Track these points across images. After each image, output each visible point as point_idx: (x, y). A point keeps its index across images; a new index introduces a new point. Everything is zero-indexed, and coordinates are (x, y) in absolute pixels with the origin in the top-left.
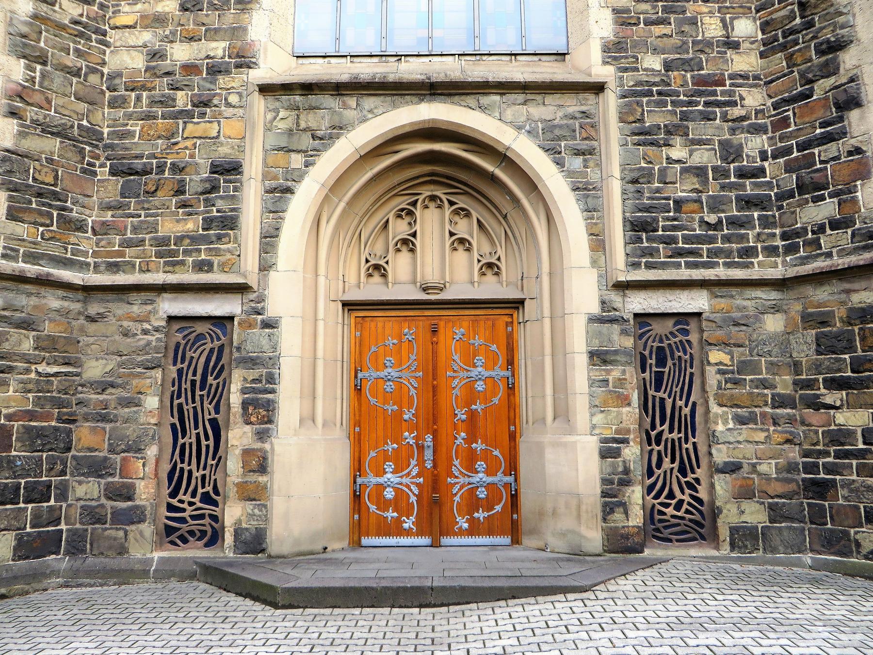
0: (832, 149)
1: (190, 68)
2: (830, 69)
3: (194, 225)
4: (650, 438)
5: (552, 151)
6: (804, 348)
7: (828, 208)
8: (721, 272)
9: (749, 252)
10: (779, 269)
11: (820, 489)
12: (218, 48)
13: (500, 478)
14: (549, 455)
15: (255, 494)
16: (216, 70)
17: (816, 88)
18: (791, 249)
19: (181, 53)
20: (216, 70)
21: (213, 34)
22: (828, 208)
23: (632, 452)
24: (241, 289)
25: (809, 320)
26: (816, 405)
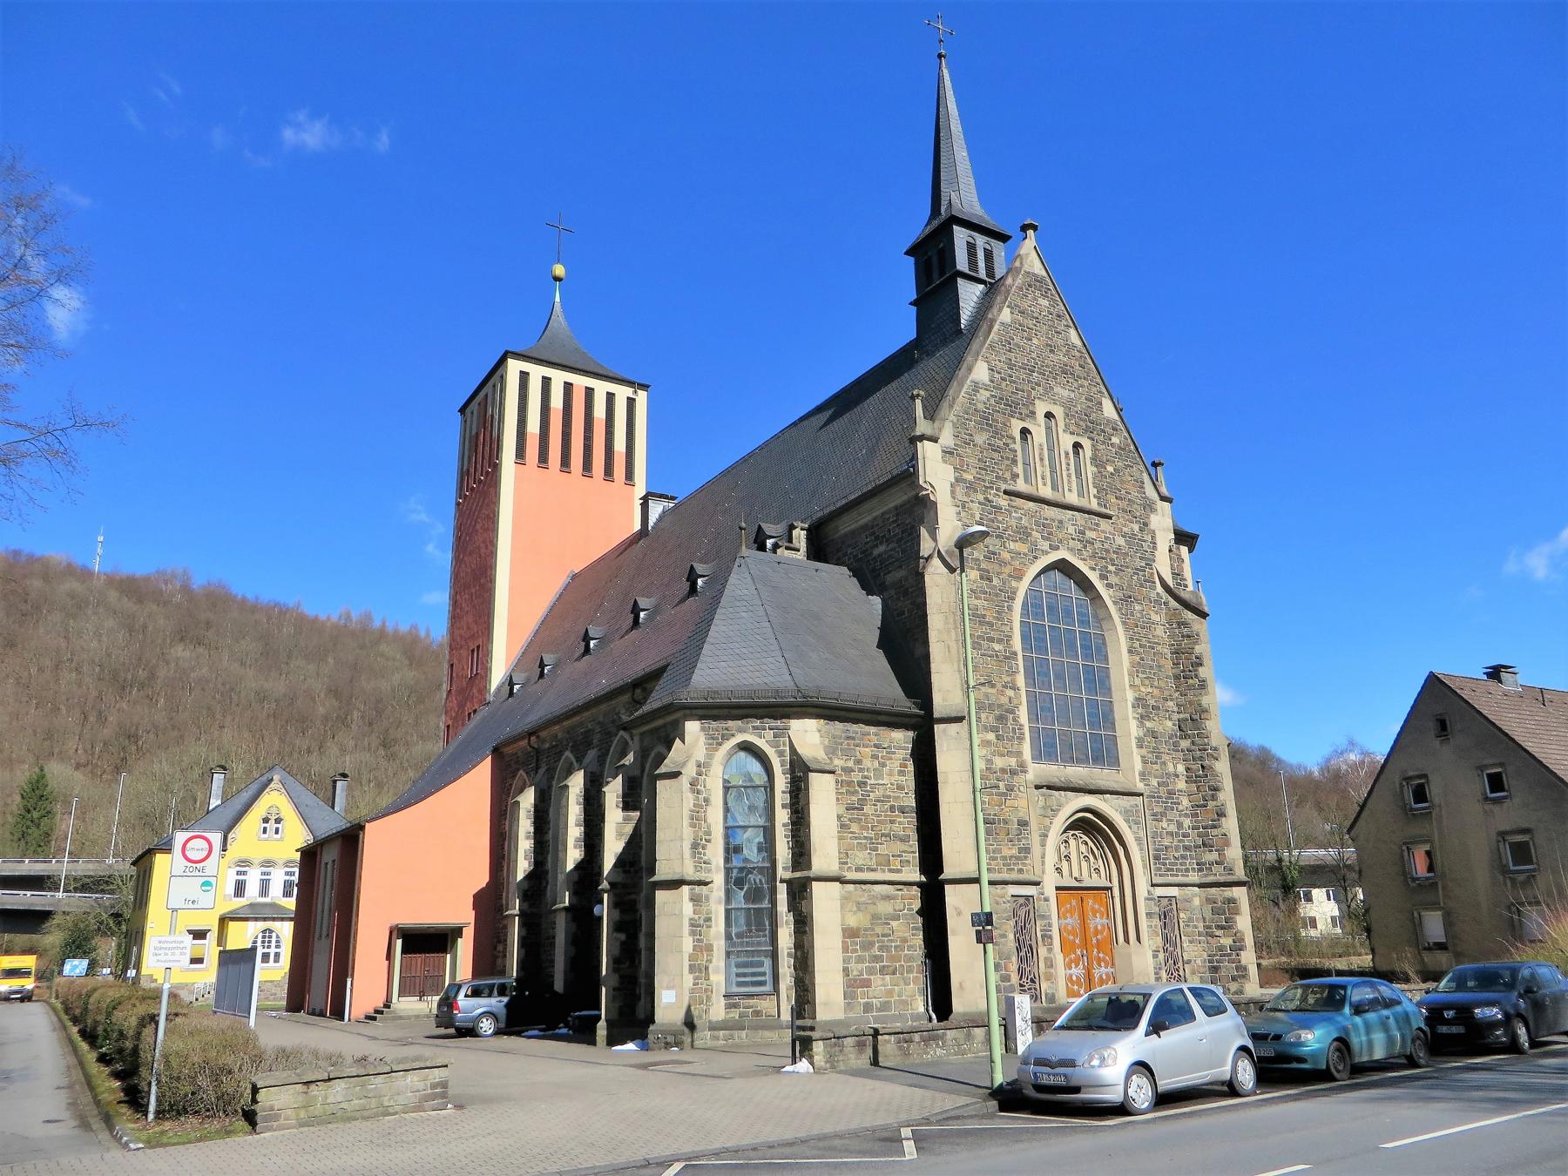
0: (1215, 832)
1: (1003, 770)
2: (1214, 798)
3: (1014, 852)
4: (1165, 951)
5: (1127, 821)
6: (1208, 914)
7: (1214, 856)
8: (1180, 879)
9: (1187, 870)
10: (1194, 877)
11: (1215, 969)
12: (1013, 762)
13: (1110, 970)
14: (1134, 958)
15: (138, 967)
16: (1013, 773)
17: (936, 471)
18: (1200, 870)
19: (999, 762)
20: (1013, 773)
21: (1009, 754)
22: (1214, 856)
23: (1161, 956)
24: (1037, 884)
25: (1208, 900)
26: (1213, 936)
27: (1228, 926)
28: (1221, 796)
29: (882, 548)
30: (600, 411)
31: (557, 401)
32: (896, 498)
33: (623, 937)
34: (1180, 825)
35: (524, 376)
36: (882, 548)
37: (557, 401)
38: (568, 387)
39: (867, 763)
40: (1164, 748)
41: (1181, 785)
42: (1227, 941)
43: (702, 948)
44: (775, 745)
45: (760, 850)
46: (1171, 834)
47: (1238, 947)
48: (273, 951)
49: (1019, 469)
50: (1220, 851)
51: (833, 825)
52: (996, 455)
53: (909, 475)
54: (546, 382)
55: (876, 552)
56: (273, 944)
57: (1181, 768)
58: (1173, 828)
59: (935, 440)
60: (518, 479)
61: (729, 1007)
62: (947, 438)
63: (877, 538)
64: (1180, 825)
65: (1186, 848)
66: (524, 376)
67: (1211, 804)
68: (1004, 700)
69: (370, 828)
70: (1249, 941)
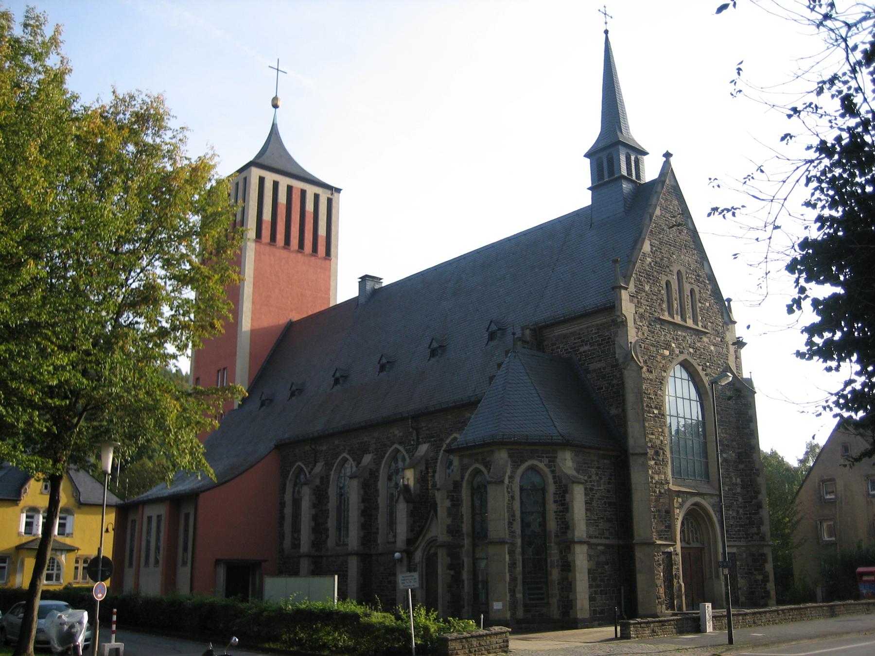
2: (756, 497)
7: (755, 530)
17: (628, 308)
27: (761, 569)
28: (760, 497)
29: (586, 348)
30: (310, 207)
31: (282, 198)
32: (600, 320)
33: (452, 572)
34: (738, 512)
35: (262, 180)
36: (586, 348)
37: (282, 198)
38: (290, 189)
39: (594, 477)
40: (731, 469)
41: (739, 490)
42: (760, 577)
43: (513, 579)
44: (549, 466)
45: (540, 525)
46: (733, 517)
47: (766, 580)
48: (55, 572)
49: (664, 306)
50: (758, 528)
51: (583, 511)
52: (655, 297)
53: (611, 308)
54: (276, 184)
55: (582, 349)
56: (55, 568)
57: (739, 480)
58: (734, 514)
59: (626, 289)
60: (258, 254)
61: (525, 611)
62: (632, 287)
63: (582, 341)
64: (738, 512)
65: (741, 526)
66: (262, 180)
67: (754, 501)
68: (658, 442)
69: (201, 495)
70: (772, 577)
